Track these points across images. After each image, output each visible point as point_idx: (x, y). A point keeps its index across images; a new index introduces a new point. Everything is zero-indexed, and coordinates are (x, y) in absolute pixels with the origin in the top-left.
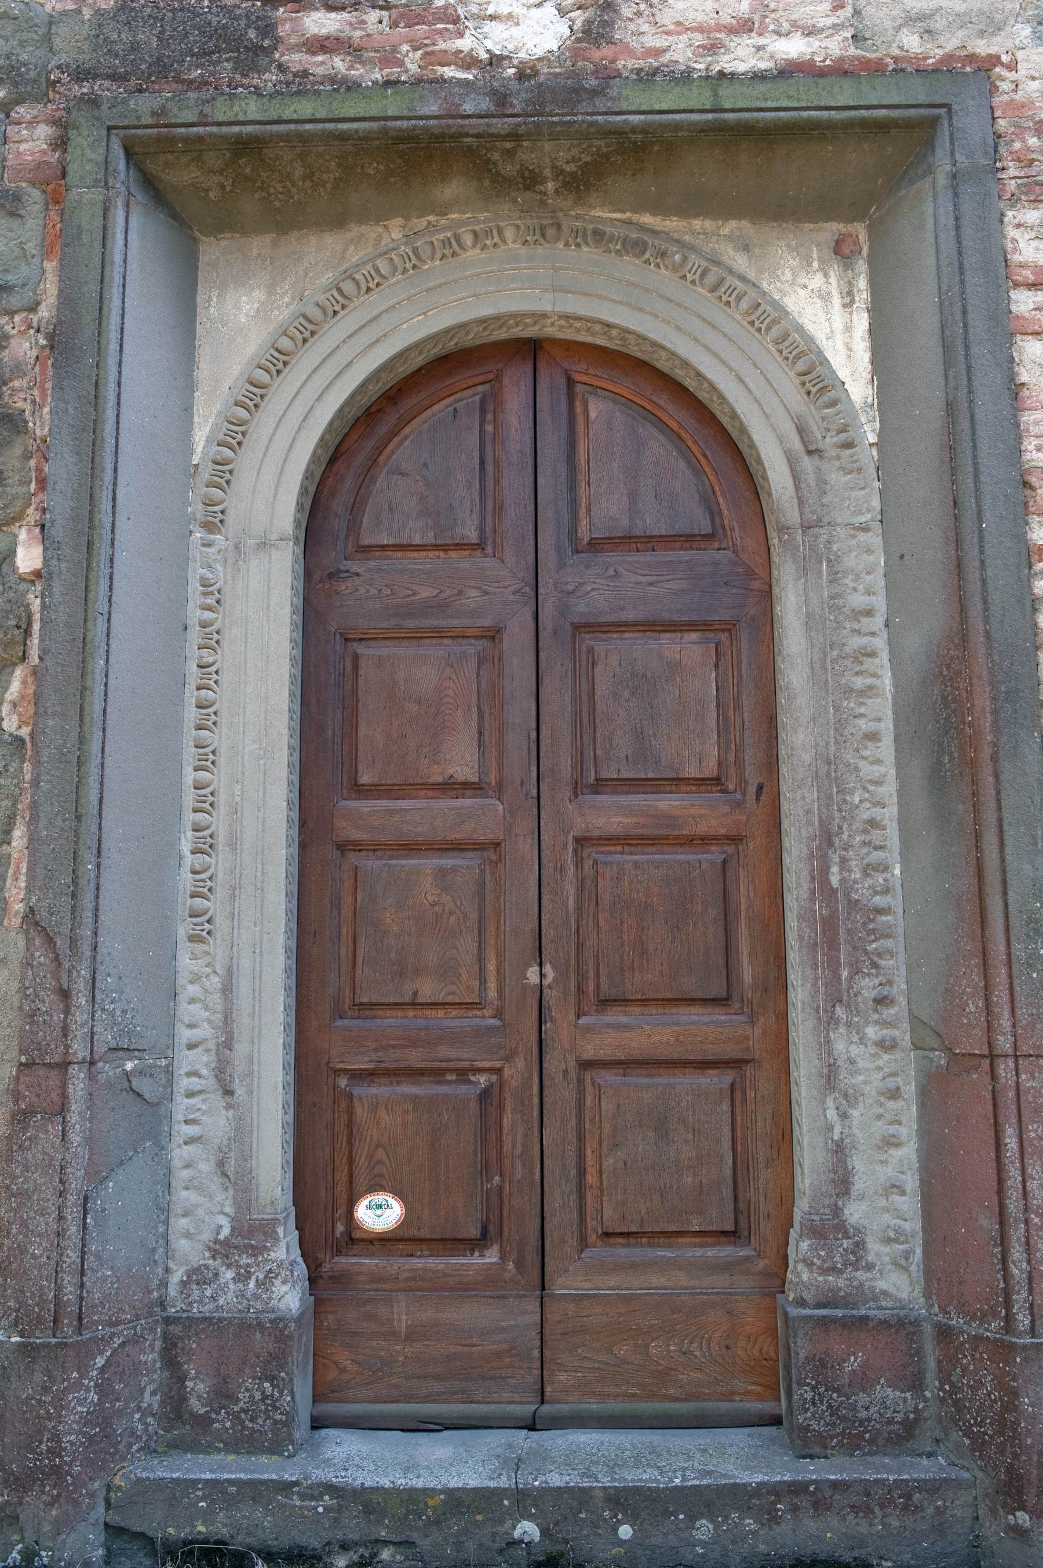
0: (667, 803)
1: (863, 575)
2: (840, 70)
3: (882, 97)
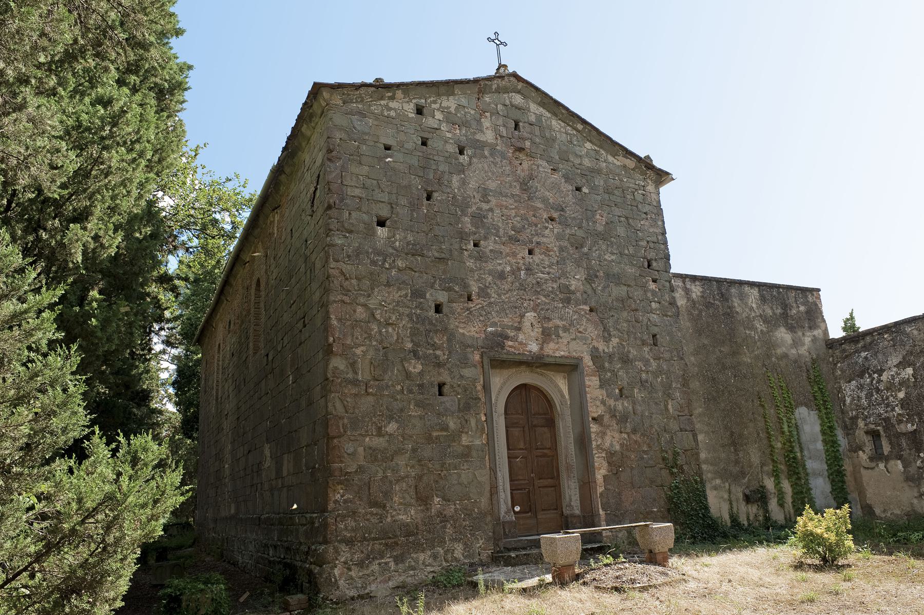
0: (545, 451)
1: (192, 279)
2: (566, 357)
3: (573, 362)
